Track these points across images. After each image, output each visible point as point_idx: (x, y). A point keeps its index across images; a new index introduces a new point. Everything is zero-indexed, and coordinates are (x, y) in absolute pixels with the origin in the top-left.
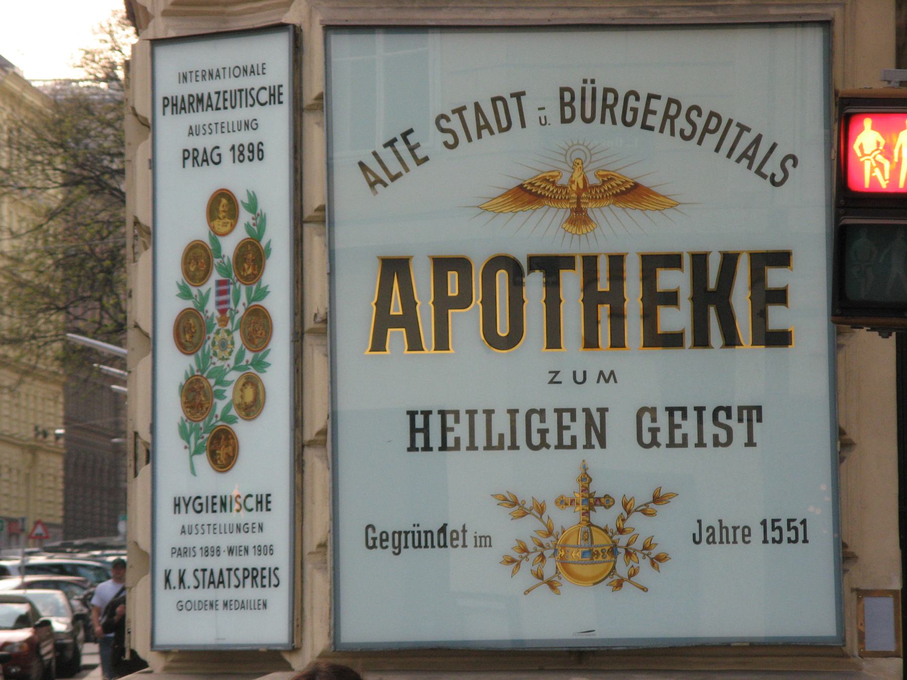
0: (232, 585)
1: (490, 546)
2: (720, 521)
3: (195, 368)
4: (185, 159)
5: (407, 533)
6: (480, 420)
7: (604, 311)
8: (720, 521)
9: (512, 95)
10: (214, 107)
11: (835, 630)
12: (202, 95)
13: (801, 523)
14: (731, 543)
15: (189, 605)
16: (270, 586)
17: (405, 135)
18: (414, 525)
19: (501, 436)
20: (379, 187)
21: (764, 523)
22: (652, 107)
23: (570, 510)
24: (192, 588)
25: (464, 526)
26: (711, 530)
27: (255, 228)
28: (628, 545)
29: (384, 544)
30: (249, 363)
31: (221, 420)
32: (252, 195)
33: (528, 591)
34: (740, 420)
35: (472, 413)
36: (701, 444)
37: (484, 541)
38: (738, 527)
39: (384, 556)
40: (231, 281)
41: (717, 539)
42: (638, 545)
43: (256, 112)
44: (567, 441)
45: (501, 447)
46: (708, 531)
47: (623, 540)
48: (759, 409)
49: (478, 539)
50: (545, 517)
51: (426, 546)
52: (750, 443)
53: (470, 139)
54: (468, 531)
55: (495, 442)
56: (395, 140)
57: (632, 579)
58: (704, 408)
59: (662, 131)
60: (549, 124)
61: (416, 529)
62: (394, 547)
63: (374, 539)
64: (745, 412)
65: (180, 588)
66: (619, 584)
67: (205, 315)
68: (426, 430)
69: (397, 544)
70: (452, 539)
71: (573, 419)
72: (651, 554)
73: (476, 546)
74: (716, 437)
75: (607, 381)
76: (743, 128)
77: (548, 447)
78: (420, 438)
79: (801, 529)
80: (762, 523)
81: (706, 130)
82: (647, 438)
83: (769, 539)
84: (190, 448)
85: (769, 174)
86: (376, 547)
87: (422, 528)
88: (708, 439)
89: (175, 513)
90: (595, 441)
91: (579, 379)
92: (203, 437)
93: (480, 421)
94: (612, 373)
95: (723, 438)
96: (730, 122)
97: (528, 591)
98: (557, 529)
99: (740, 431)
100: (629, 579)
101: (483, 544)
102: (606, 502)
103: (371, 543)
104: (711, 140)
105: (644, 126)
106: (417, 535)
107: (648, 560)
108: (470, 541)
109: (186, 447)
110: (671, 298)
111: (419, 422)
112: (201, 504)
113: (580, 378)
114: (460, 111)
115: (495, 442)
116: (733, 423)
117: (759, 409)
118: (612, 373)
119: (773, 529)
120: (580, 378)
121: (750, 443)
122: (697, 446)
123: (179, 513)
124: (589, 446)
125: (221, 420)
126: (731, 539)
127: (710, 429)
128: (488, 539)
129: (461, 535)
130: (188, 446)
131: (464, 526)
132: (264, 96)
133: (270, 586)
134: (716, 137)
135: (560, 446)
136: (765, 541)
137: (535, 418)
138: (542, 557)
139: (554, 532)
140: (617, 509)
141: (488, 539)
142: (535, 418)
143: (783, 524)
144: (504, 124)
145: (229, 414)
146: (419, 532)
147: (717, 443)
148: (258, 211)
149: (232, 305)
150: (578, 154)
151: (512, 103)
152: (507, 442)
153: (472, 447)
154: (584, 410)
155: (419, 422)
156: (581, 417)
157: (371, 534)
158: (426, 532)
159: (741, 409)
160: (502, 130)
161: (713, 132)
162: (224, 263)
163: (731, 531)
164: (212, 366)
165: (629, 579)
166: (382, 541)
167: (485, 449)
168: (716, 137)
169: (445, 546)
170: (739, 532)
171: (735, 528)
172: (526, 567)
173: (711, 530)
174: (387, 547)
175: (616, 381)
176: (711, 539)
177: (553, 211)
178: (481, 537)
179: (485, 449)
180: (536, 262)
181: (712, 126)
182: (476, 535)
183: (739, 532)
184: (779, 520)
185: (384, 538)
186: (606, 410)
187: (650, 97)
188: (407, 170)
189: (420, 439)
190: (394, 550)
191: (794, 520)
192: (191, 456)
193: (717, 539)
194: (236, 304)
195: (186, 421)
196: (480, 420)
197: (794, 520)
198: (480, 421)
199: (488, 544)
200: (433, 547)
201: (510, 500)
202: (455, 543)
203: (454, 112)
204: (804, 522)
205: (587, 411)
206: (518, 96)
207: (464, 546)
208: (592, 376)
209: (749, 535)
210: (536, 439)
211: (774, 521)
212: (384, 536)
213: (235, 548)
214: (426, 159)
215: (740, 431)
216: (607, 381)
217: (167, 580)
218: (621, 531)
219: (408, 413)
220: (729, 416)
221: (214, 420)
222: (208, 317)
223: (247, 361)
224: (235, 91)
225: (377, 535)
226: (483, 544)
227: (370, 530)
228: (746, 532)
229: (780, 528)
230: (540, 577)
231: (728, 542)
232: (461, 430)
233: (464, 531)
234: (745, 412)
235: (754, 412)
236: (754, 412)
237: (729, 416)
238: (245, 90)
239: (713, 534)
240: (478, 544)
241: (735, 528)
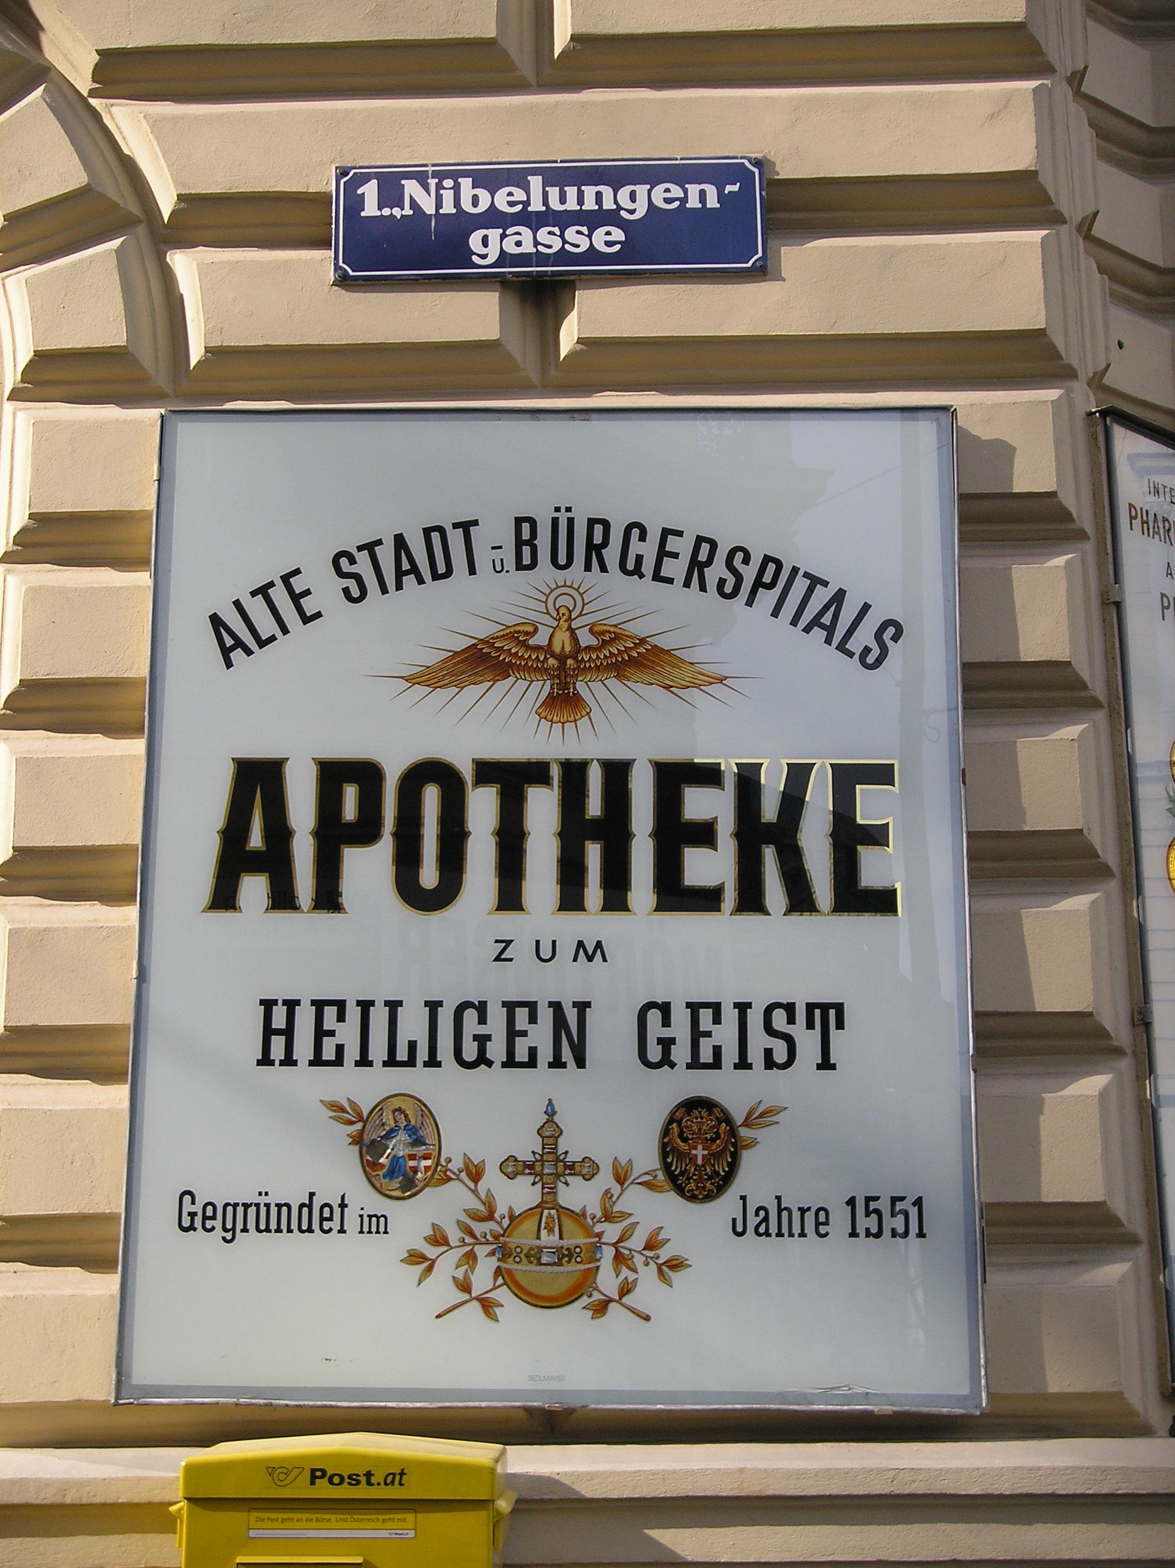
1: (386, 1232)
2: (778, 1198)
5: (246, 1206)
6: (379, 1016)
7: (593, 853)
8: (778, 1198)
9: (456, 526)
13: (914, 1204)
14: (796, 1235)
17: (286, 579)
18: (260, 1194)
19: (412, 1046)
20: (237, 655)
21: (851, 1202)
22: (669, 548)
23: (524, 1181)
25: (343, 1197)
26: (762, 1213)
28: (621, 1240)
29: (209, 1224)
34: (810, 1025)
35: (365, 1006)
36: (743, 1064)
38: (809, 1209)
39: (206, 1243)
41: (773, 1229)
42: (637, 1242)
44: (521, 1055)
45: (411, 1062)
46: (757, 1215)
47: (611, 1232)
48: (839, 1008)
49: (366, 1220)
50: (482, 1186)
51: (279, 1230)
52: (826, 1064)
53: (384, 590)
55: (402, 1054)
56: (271, 584)
57: (624, 1300)
58: (749, 1005)
59: (687, 584)
60: (507, 572)
61: (262, 1200)
62: (225, 1230)
63: (192, 1215)
64: (817, 1012)
66: (601, 1308)
68: (288, 1032)
69: (229, 1226)
70: (322, 1219)
71: (533, 1019)
72: (658, 1257)
73: (361, 1232)
74: (768, 1053)
75: (590, 958)
76: (815, 581)
77: (489, 1064)
78: (278, 1043)
79: (913, 1212)
80: (848, 1203)
81: (758, 584)
82: (655, 1053)
83: (860, 1230)
85: (858, 651)
86: (195, 1229)
87: (272, 1200)
88: (755, 1056)
90: (567, 1055)
91: (545, 954)
93: (379, 1018)
94: (599, 945)
95: (780, 1056)
96: (795, 570)
98: (501, 1210)
99: (808, 1042)
100: (620, 1299)
101: (374, 1229)
102: (587, 1169)
103: (186, 1222)
104: (767, 599)
105: (657, 577)
106: (263, 1210)
107: (653, 1267)
108: (352, 1223)
110: (704, 834)
111: (279, 1019)
113: (546, 953)
114: (370, 548)
115: (402, 1054)
116: (798, 1031)
117: (839, 1008)
118: (599, 945)
119: (868, 1214)
120: (546, 953)
121: (826, 1064)
122: (737, 1067)
124: (557, 1063)
126: (796, 1230)
127: (758, 1041)
128: (382, 1220)
129: (337, 1212)
131: (343, 1197)
134: (773, 595)
135: (510, 1062)
136: (854, 1234)
137: (470, 1016)
138: (470, 1258)
139: (497, 1215)
140: (605, 1180)
141: (382, 1220)
142: (470, 1016)
143: (884, 1205)
144: (442, 569)
146: (267, 1205)
147: (770, 1063)
150: (566, 601)
151: (456, 539)
152: (422, 1054)
153: (364, 1061)
154: (551, 1004)
155: (279, 1019)
156: (546, 1016)
157: (187, 1207)
158: (279, 1206)
159: (810, 1007)
160: (436, 576)
161: (771, 586)
163: (796, 1215)
165: (620, 1299)
166: (205, 1218)
167: (385, 1064)
168: (773, 595)
169: (310, 1230)
170: (810, 1217)
171: (803, 1211)
172: (448, 1264)
173: (762, 1213)
174: (213, 1228)
175: (605, 960)
176: (762, 1229)
177: (522, 684)
178: (370, 1217)
179: (385, 1064)
180: (487, 771)
181: (767, 578)
182: (362, 1212)
183: (810, 1217)
184: (876, 1199)
185: (209, 1213)
186: (588, 1004)
187: (666, 532)
188: (285, 631)
189: (278, 1045)
190: (225, 1234)
191: (902, 1199)
193: (773, 1229)
196: (379, 1016)
197: (902, 1199)
198: (379, 1018)
199: (382, 1229)
200: (290, 1231)
202: (326, 1225)
203: (360, 548)
204: (918, 1202)
205: (556, 1007)
206: (466, 527)
207: (342, 1231)
208: (567, 949)
209: (826, 1223)
210: (470, 1051)
211: (868, 1199)
212: (209, 1212)
214: (318, 615)
215: (808, 1042)
216: (590, 958)
218: (608, 1217)
219: (262, 1002)
220: (791, 1020)
225: (198, 1208)
226: (374, 1229)
227: (187, 1198)
228: (822, 1218)
229: (878, 1212)
230: (464, 1286)
231: (791, 1235)
232: (347, 1034)
233: (343, 1206)
234: (817, 1012)
235: (832, 1012)
236: (832, 1012)
237: (791, 1020)
239: (766, 1219)
240: (366, 1229)
241: (803, 1211)
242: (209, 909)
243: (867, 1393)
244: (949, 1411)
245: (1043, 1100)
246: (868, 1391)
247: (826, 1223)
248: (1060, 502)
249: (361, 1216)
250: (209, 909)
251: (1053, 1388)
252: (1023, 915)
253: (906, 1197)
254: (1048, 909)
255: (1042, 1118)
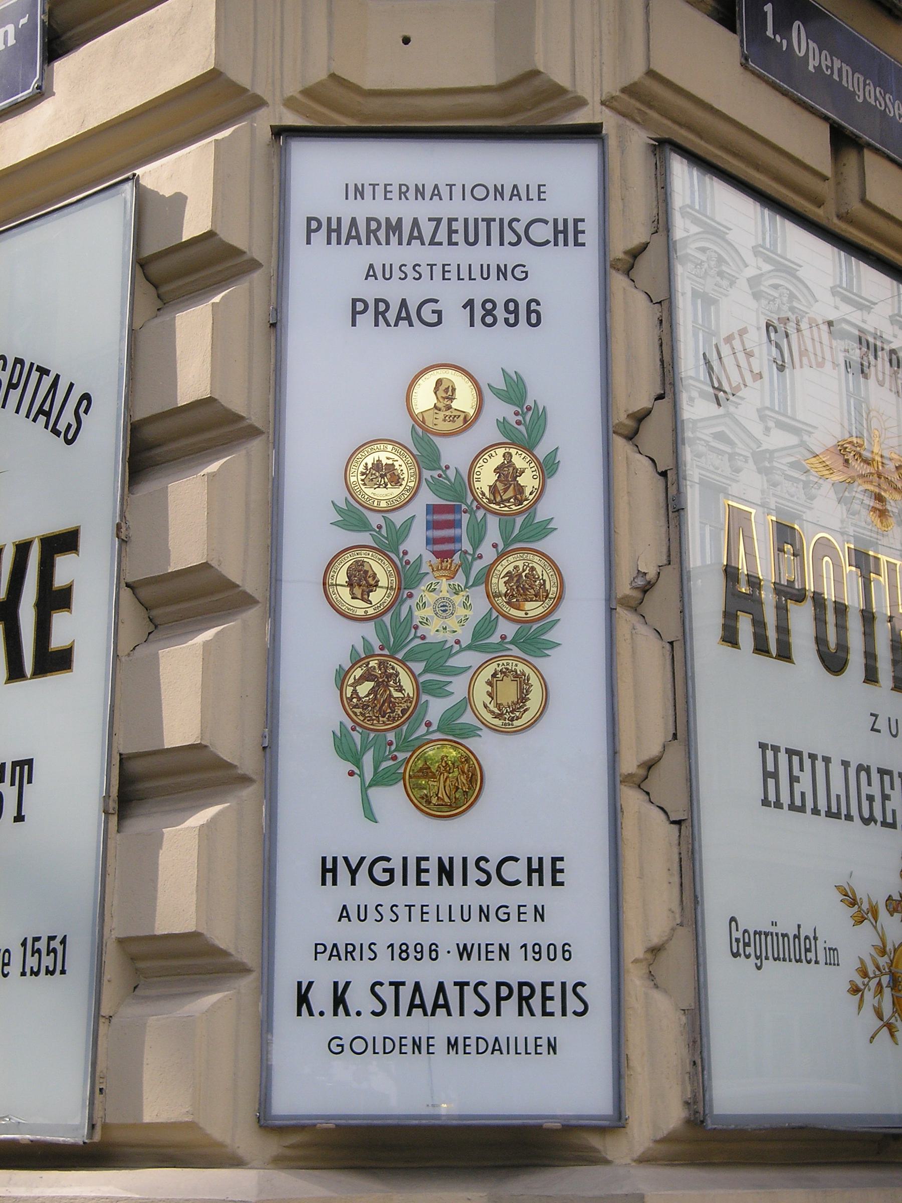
0: (469, 1008)
3: (376, 643)
4: (354, 313)
10: (427, 240)
11: (611, 1108)
12: (400, 220)
15: (359, 1046)
16: (564, 1013)
24: (366, 1014)
27: (522, 428)
30: (508, 640)
31: (439, 730)
32: (515, 377)
33: (873, 1037)
37: (832, 956)
40: (464, 507)
43: (524, 253)
49: (828, 951)
54: (819, 939)
65: (335, 1014)
67: (401, 560)
84: (362, 776)
89: (324, 883)
92: (394, 758)
97: (873, 1037)
109: (351, 774)
112: (391, 871)
123: (335, 883)
125: (439, 730)
130: (357, 771)
132: (541, 232)
133: (564, 1013)
143: (42, 945)
145: (462, 720)
148: (529, 402)
149: (466, 545)
162: (447, 478)
164: (418, 641)
192: (364, 790)
194: (476, 542)
195: (353, 729)
201: (851, 896)
209: (8, 964)
213: (476, 947)
217: (303, 999)
221: (423, 729)
222: (408, 562)
223: (503, 637)
224: (476, 220)
238: (498, 220)
242: (32, 541)
243: (19, 1123)
244: (63, 1141)
245: (163, 834)
246: (21, 1121)
247: (8, 964)
248: (220, 239)
249: (825, 948)
250: (32, 541)
251: (149, 1116)
252: (160, 656)
253: (56, 936)
254: (186, 644)
255: (161, 852)
